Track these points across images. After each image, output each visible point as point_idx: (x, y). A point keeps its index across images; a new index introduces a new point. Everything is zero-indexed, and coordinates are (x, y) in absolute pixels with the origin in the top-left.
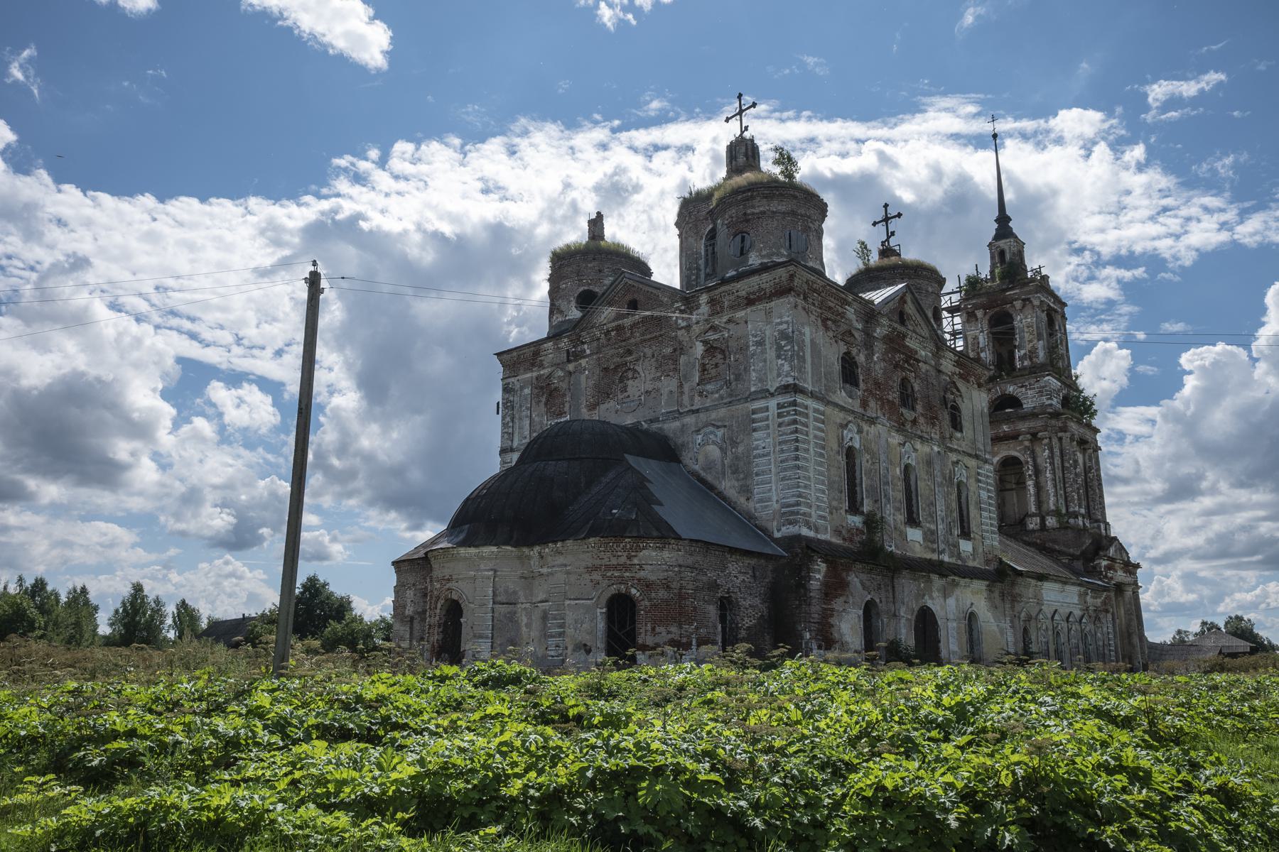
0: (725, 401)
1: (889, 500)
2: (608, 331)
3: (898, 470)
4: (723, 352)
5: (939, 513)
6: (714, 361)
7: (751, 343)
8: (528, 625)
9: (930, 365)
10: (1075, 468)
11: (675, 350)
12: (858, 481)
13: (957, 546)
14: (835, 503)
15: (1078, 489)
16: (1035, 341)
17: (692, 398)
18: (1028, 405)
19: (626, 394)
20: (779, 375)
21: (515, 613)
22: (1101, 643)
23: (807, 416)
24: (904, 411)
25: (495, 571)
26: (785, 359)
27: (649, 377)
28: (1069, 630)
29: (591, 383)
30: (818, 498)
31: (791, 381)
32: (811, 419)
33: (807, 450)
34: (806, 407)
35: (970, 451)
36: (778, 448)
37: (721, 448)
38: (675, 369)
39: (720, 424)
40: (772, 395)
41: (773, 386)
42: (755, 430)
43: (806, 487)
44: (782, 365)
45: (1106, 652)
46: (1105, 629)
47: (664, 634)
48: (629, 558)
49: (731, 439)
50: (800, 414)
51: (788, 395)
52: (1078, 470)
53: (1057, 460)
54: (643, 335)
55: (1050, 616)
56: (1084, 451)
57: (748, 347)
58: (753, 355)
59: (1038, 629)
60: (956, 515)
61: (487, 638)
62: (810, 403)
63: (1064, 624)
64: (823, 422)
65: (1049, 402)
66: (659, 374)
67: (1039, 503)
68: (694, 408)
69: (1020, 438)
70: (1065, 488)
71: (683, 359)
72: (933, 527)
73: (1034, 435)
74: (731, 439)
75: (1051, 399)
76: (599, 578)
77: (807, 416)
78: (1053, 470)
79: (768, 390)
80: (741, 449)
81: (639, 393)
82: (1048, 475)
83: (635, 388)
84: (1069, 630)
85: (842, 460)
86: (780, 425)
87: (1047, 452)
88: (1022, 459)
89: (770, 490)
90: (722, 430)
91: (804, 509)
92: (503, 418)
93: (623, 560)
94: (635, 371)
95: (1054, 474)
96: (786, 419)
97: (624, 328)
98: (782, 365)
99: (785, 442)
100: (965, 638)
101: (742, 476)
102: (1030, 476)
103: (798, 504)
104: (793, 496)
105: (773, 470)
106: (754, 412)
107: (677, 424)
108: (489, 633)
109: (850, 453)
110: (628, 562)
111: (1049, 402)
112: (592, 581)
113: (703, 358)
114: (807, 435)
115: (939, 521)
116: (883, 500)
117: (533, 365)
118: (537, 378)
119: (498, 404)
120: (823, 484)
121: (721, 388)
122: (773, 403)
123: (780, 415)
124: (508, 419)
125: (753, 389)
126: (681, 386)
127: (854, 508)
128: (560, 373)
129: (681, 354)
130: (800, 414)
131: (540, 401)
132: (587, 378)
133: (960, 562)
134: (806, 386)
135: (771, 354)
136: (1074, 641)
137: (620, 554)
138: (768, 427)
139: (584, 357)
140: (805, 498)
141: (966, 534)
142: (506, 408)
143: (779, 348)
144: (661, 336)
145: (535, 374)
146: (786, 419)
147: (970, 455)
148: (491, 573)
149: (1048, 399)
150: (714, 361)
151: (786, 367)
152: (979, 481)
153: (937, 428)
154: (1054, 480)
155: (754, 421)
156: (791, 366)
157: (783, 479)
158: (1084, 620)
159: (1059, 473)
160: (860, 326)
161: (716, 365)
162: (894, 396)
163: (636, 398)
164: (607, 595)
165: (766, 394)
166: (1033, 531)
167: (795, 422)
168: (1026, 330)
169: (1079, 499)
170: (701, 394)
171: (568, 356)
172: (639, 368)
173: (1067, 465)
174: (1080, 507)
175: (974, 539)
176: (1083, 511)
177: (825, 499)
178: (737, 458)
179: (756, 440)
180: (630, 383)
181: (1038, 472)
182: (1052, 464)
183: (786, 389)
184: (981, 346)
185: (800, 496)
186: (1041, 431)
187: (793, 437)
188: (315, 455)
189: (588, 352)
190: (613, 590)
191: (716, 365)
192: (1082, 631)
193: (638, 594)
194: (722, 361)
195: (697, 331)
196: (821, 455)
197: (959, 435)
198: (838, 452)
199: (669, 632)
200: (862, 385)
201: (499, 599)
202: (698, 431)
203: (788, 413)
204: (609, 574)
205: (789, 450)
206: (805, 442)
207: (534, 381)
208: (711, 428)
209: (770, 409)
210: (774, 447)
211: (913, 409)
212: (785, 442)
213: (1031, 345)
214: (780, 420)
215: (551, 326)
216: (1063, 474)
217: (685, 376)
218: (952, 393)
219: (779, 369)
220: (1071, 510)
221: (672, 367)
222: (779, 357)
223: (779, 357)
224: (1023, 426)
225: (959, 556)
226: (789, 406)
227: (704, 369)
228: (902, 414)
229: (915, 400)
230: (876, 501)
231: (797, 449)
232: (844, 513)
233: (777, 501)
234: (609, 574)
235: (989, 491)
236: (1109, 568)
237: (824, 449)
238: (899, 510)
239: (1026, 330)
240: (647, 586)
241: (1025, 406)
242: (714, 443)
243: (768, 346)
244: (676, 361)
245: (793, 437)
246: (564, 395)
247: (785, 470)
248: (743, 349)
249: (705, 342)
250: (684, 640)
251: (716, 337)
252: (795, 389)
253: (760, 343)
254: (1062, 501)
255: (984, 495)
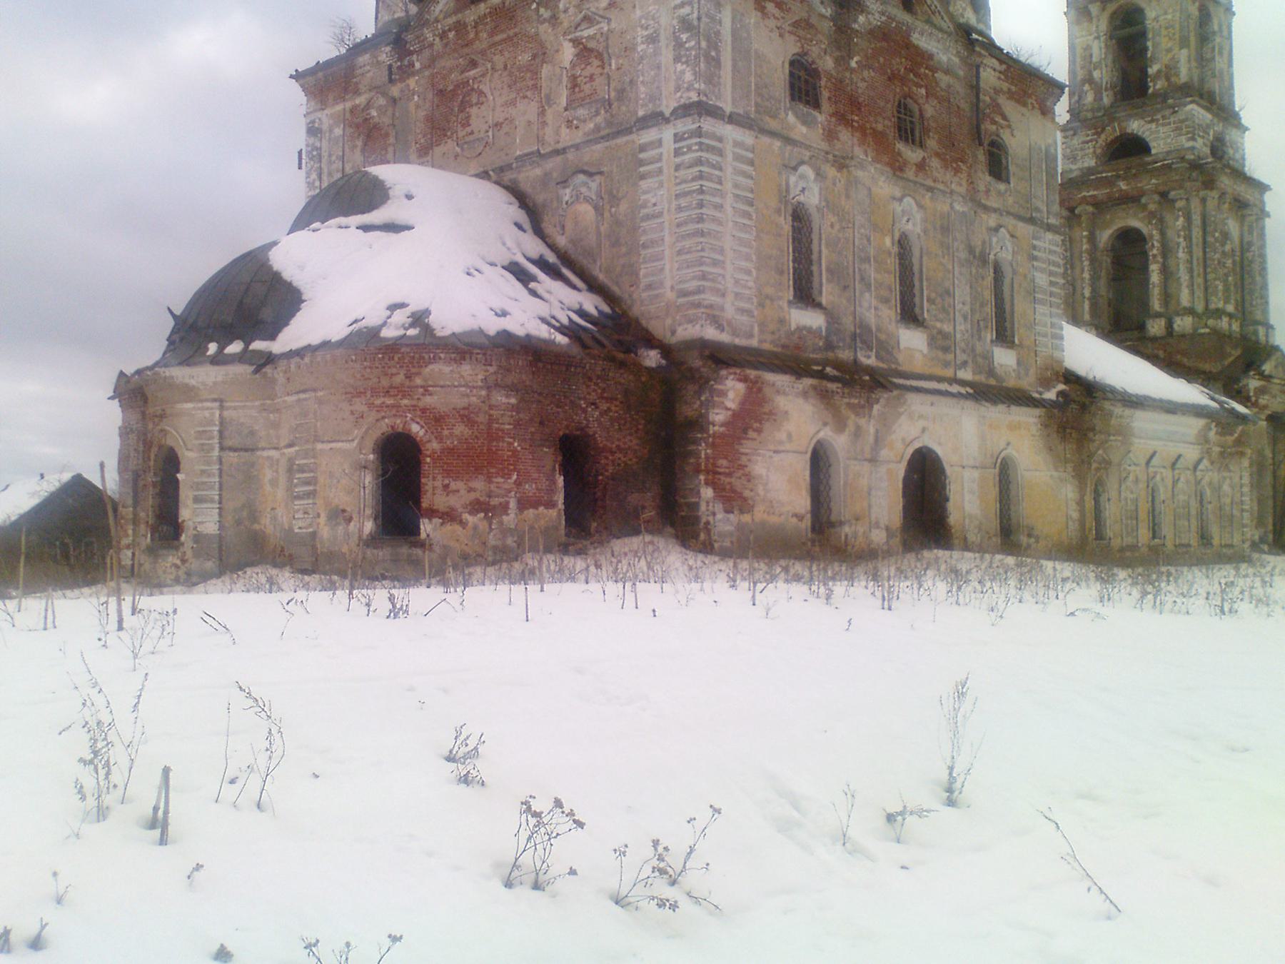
0: (603, 133)
1: (868, 286)
2: (444, 32)
3: (888, 241)
4: (599, 56)
5: (959, 306)
6: (587, 72)
7: (639, 40)
8: (274, 483)
9: (956, 77)
10: (1223, 245)
11: (534, 57)
12: (815, 257)
13: (988, 357)
14: (769, 291)
15: (1226, 275)
16: (1176, 50)
17: (557, 133)
18: (1158, 147)
19: (469, 129)
20: (678, 89)
21: (253, 465)
22: (1228, 501)
23: (720, 153)
24: (900, 146)
25: (221, 401)
26: (686, 62)
27: (500, 101)
28: (1175, 482)
29: (422, 114)
30: (737, 282)
31: (694, 97)
32: (730, 157)
33: (719, 207)
34: (720, 140)
35: (1022, 213)
36: (674, 204)
37: (596, 208)
38: (535, 87)
39: (593, 170)
40: (667, 121)
41: (667, 106)
42: (643, 177)
43: (715, 263)
44: (683, 72)
45: (1236, 512)
46: (1236, 480)
47: (463, 492)
48: (408, 377)
49: (610, 193)
50: (710, 149)
51: (689, 120)
52: (1228, 248)
53: (1197, 233)
54: (492, 34)
55: (1143, 462)
56: (1242, 219)
57: (634, 48)
58: (642, 58)
59: (1122, 481)
60: (990, 310)
61: (212, 501)
62: (730, 132)
63: (1168, 473)
64: (751, 163)
65: (1191, 144)
66: (513, 95)
67: (1167, 297)
68: (560, 146)
69: (1143, 200)
70: (1205, 273)
71: (545, 70)
72: (947, 328)
73: (1164, 195)
74: (610, 193)
75: (1193, 139)
76: (364, 408)
77: (720, 153)
78: (1190, 247)
79: (661, 114)
80: (623, 207)
81: (485, 127)
82: (1181, 255)
83: (481, 118)
84: (1175, 482)
85: (786, 225)
86: (677, 168)
87: (1181, 221)
88: (1145, 230)
89: (662, 270)
90: (597, 178)
91: (710, 298)
92: (308, 175)
93: (399, 379)
94: (481, 93)
95: (1190, 253)
96: (688, 158)
97: (465, 25)
98: (683, 72)
99: (685, 194)
100: (994, 492)
101: (624, 250)
102: (1154, 256)
103: (699, 291)
104: (694, 278)
105: (667, 239)
106: (643, 148)
107: (538, 172)
108: (214, 494)
109: (800, 217)
110: (407, 383)
111: (1191, 144)
112: (352, 413)
113: (573, 65)
114: (720, 183)
115: (959, 319)
116: (858, 286)
117: (346, 90)
118: (352, 111)
119: (300, 153)
120: (748, 258)
121: (597, 113)
122: (667, 133)
123: (677, 152)
124: (314, 176)
125: (641, 113)
126: (542, 113)
127: (805, 295)
128: (382, 101)
129: (543, 62)
130: (710, 149)
131: (355, 146)
132: (418, 107)
133: (992, 382)
134: (719, 104)
135: (667, 55)
136: (1182, 497)
137: (394, 371)
138: (660, 171)
139: (413, 74)
140: (713, 280)
141: (1004, 336)
142: (311, 159)
143: (679, 45)
144: (516, 35)
145: (348, 105)
146: (688, 158)
147: (1019, 218)
148: (217, 404)
149: (1189, 140)
150: (589, 70)
151: (688, 76)
152: (1035, 258)
153: (964, 176)
154: (1190, 262)
155: (642, 163)
156: (695, 74)
157: (679, 253)
158: (1201, 467)
159: (1198, 252)
160: (828, 12)
161: (591, 78)
162: (884, 124)
163: (482, 135)
164: (376, 434)
165: (657, 118)
166: (1154, 339)
167: (699, 162)
168: (1164, 32)
169: (1226, 289)
170: (569, 123)
171: (390, 73)
172: (485, 88)
173: (1210, 239)
174: (1227, 301)
175: (1021, 345)
176: (1230, 308)
177: (751, 284)
178: (618, 223)
179: (645, 192)
180: (474, 111)
181: (1166, 251)
182: (1188, 238)
183: (685, 110)
184: (1095, 59)
185: (703, 277)
186: (1174, 189)
187: (695, 185)
188: (1019, 340)
189: (417, 65)
190: (384, 427)
191: (591, 78)
192: (1198, 482)
193: (422, 433)
194: (599, 70)
195: (566, 24)
196: (747, 215)
197: (1002, 187)
198: (778, 211)
199: (470, 490)
200: (825, 105)
201: (229, 443)
202: (564, 182)
203: (689, 148)
204: (378, 402)
205: (688, 208)
206: (716, 193)
207: (348, 115)
208: (581, 177)
209: (665, 142)
210: (670, 203)
211: (921, 145)
212: (685, 194)
213: (1170, 56)
214: (678, 160)
215: (376, 28)
216: (1205, 252)
217: (548, 97)
218: (994, 122)
219: (679, 78)
220: (1212, 306)
221: (530, 83)
222: (677, 59)
223: (677, 59)
224: (1149, 183)
225: (991, 372)
226: (690, 138)
227: (574, 85)
228: (899, 154)
229: (925, 131)
230: (845, 288)
231: (701, 205)
232: (785, 305)
233: (672, 288)
234: (378, 402)
235: (1051, 274)
236: (1261, 391)
237: (751, 204)
238: (886, 301)
239: (1164, 32)
240: (436, 420)
241: (1153, 151)
242: (587, 200)
243: (663, 43)
244: (536, 74)
245: (695, 185)
246: (387, 135)
247: (683, 237)
248: (629, 49)
249: (576, 42)
250: (495, 501)
251: (591, 32)
252: (701, 109)
253: (653, 39)
254: (1199, 293)
255: (1042, 280)
